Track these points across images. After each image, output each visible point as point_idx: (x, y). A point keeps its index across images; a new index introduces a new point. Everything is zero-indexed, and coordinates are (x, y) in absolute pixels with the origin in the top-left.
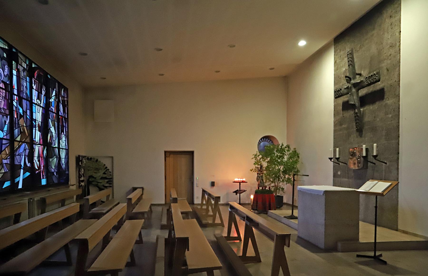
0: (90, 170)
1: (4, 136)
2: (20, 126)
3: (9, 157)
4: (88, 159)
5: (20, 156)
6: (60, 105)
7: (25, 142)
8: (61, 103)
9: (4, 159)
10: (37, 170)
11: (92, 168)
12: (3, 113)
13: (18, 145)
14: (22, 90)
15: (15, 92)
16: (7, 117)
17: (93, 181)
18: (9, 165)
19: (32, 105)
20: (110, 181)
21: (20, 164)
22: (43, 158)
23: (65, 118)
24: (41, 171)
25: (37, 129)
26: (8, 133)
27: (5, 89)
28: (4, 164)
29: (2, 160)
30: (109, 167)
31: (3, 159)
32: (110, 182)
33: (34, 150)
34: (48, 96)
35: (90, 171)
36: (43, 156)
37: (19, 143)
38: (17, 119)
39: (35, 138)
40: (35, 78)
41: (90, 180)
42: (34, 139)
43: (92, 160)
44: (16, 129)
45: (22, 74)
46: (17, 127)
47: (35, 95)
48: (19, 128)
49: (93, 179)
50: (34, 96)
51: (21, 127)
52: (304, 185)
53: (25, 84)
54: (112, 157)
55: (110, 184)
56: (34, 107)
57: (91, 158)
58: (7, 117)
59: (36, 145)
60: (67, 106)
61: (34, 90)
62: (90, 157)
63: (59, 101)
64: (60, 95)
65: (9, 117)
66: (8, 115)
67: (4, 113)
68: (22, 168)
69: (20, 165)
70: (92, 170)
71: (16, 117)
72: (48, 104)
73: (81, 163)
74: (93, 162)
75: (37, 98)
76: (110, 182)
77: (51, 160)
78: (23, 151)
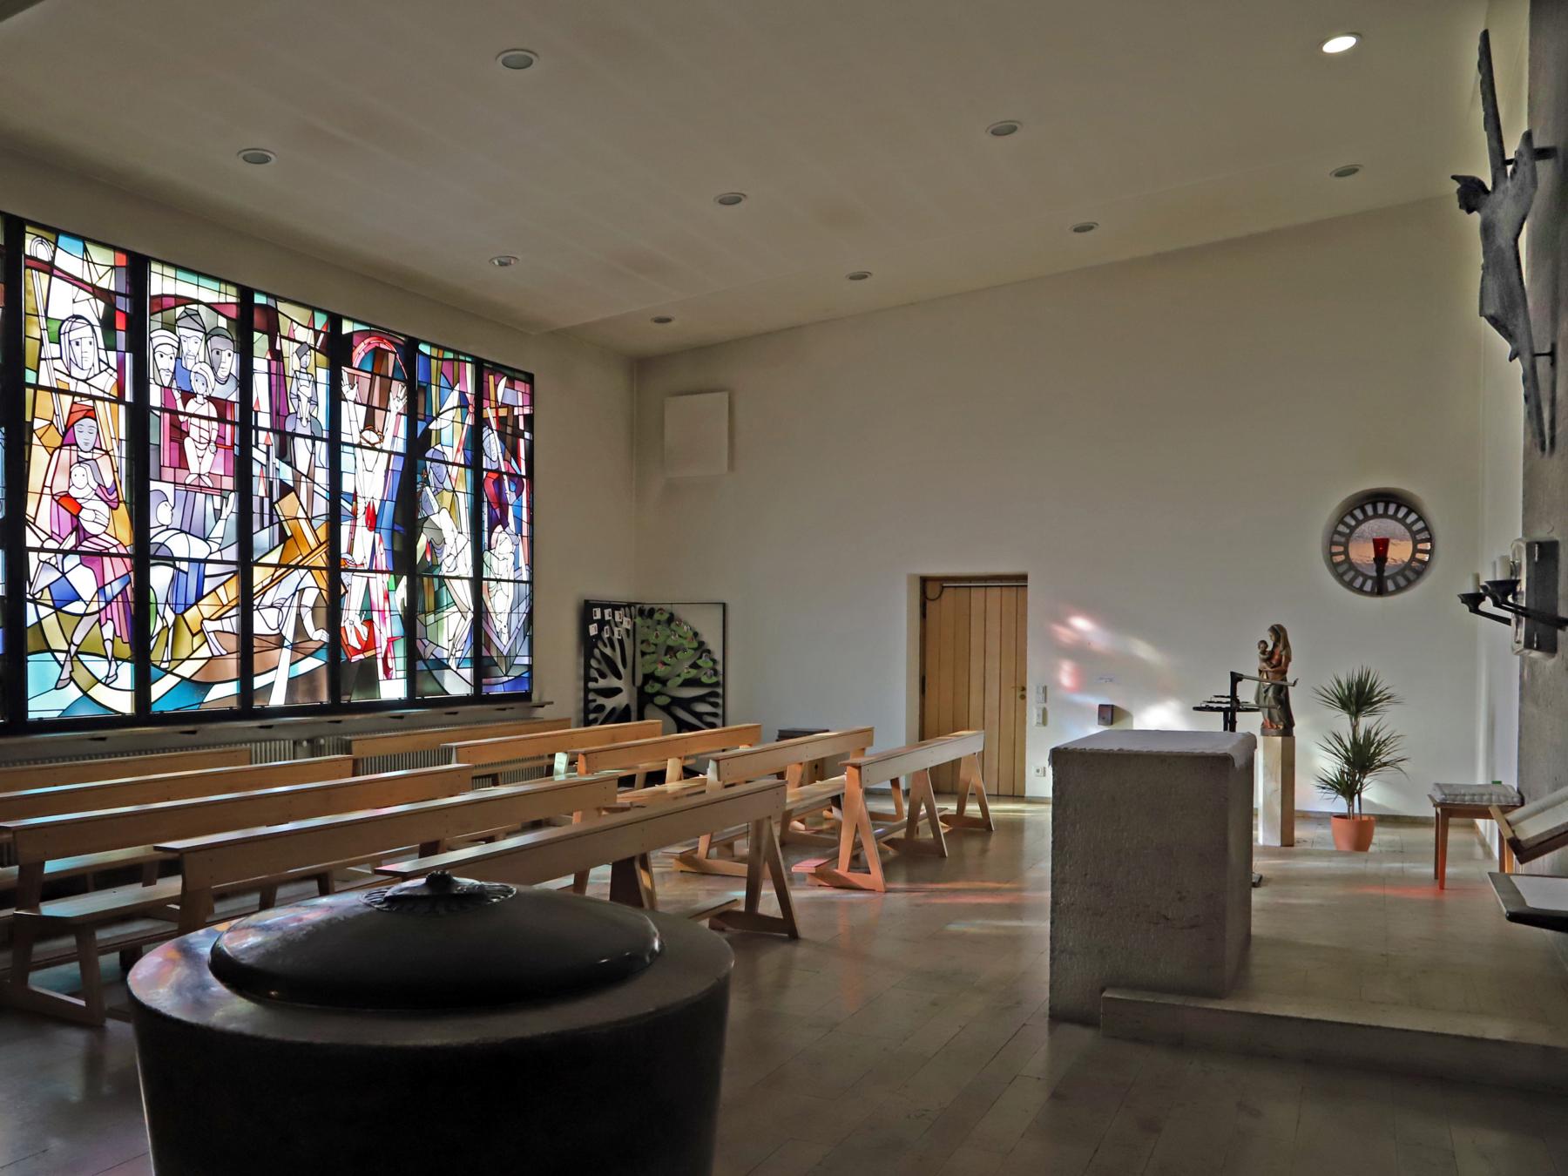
0: (649, 653)
1: (211, 553)
2: (282, 518)
3: (233, 612)
4: (641, 612)
5: (280, 610)
6: (484, 435)
7: (303, 567)
8: (490, 428)
9: (209, 619)
10: (357, 652)
11: (656, 645)
12: (209, 487)
13: (273, 575)
14: (292, 410)
15: (264, 420)
16: (224, 498)
17: (659, 693)
18: (235, 637)
19: (339, 452)
20: (715, 693)
21: (277, 631)
22: (387, 613)
23: (513, 477)
24: (379, 656)
25: (361, 520)
26: (234, 541)
27: (221, 419)
28: (212, 635)
29: (202, 623)
30: (713, 643)
31: (204, 619)
32: (712, 700)
33: (343, 591)
34: (417, 412)
35: (648, 657)
36: (387, 608)
37: (276, 571)
38: (266, 501)
39: (350, 552)
40: (356, 364)
41: (649, 689)
42: (344, 555)
43: (657, 616)
44: (263, 528)
45: (292, 364)
46: (266, 523)
47: (353, 418)
48: (277, 526)
49: (658, 686)
50: (112, 438)
51: (284, 523)
52: (879, 820)
53: (307, 391)
54: (724, 605)
55: (715, 705)
56: (344, 457)
57: (651, 612)
58: (224, 498)
59: (355, 574)
60: (527, 435)
61: (351, 404)
62: (647, 607)
63: (480, 423)
64: (486, 402)
65: (232, 496)
66: (231, 491)
67: (213, 488)
68: (286, 643)
69: (278, 634)
70: (653, 653)
71: (262, 493)
72: (419, 444)
73: (1514, 598)
74: (659, 622)
75: (365, 425)
76: (712, 700)
77: (431, 618)
78: (294, 594)
